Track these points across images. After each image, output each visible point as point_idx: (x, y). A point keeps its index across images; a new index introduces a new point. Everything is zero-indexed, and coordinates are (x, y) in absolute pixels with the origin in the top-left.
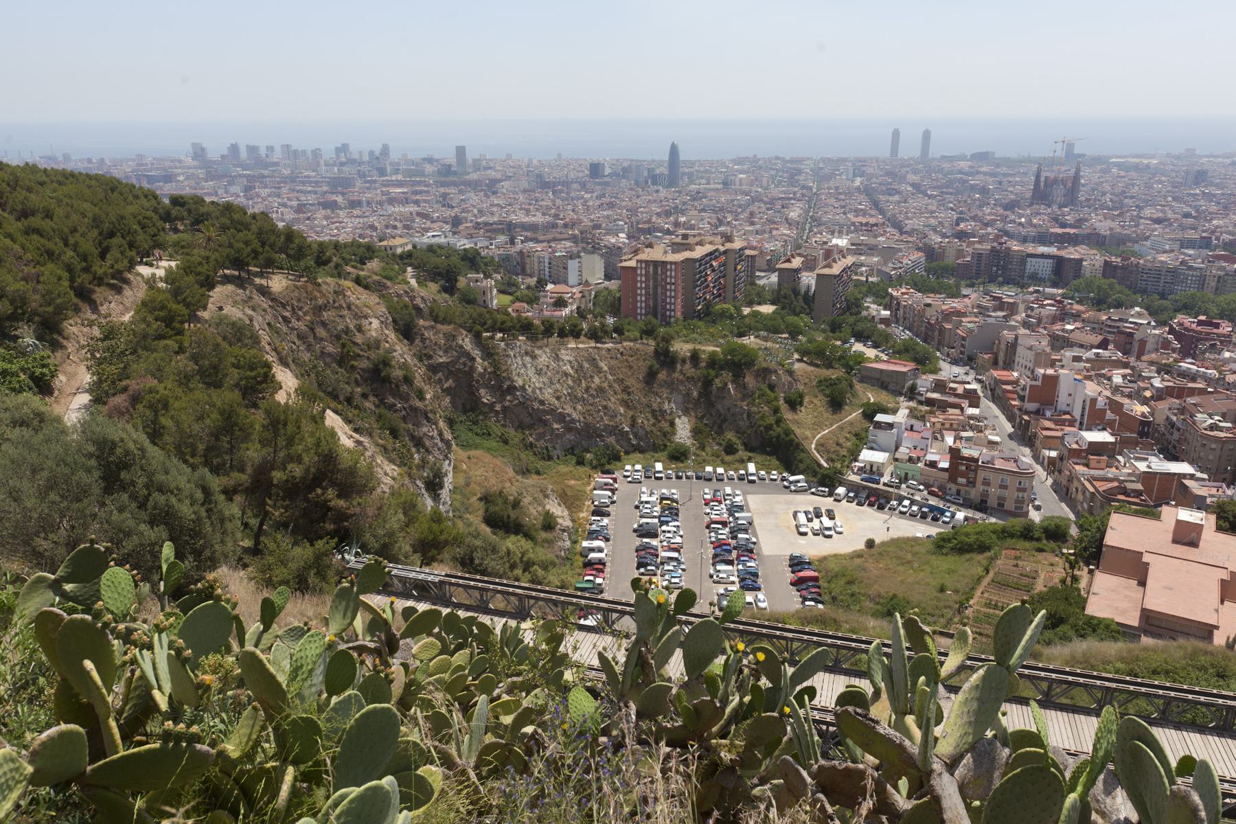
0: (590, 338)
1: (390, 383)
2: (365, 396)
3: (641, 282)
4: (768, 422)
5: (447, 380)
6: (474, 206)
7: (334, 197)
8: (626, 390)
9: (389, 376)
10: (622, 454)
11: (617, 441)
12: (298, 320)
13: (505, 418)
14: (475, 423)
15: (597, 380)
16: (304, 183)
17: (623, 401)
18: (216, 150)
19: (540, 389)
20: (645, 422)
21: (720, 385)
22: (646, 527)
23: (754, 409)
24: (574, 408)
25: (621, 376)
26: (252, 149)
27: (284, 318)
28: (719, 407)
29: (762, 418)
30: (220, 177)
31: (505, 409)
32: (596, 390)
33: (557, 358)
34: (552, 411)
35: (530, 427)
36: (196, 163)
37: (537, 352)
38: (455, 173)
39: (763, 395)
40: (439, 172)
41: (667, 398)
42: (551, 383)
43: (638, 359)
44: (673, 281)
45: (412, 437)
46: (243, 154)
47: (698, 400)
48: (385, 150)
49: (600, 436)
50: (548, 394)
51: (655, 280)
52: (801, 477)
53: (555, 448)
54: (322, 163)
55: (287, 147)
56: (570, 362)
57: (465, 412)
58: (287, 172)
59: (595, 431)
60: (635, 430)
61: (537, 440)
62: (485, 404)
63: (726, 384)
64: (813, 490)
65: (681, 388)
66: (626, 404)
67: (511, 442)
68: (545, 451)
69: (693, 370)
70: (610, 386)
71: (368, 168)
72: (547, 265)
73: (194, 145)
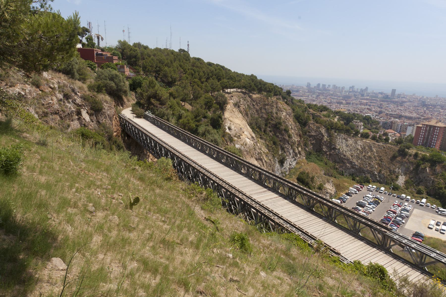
1: (279, 129)
3: (423, 132)
4: (441, 186)
5: (313, 140)
6: (390, 109)
7: (342, 101)
8: (381, 160)
9: (279, 127)
10: (371, 181)
11: (371, 177)
12: (257, 106)
13: (330, 157)
15: (369, 154)
16: (335, 96)
17: (378, 163)
18: (313, 85)
19: (346, 151)
20: (385, 173)
21: (423, 167)
22: (361, 203)
23: (436, 180)
24: (357, 161)
25: (381, 155)
26: (324, 85)
27: (253, 104)
28: (421, 176)
29: (438, 184)
30: (311, 92)
31: (330, 154)
32: (368, 157)
33: (356, 143)
34: (348, 160)
35: (338, 163)
36: (307, 88)
37: (348, 139)
38: (389, 98)
40: (383, 97)
41: (398, 167)
42: (351, 150)
43: (390, 151)
44: (437, 134)
45: (281, 147)
47: (412, 171)
48: (367, 88)
49: (364, 173)
50: (348, 154)
51: (429, 133)
53: (346, 172)
54: (344, 91)
55: (334, 86)
56: (361, 145)
57: (316, 152)
58: (331, 93)
59: (363, 171)
61: (339, 167)
62: (324, 151)
63: (426, 167)
65: (406, 165)
66: (379, 165)
67: (328, 164)
68: (341, 172)
69: (414, 160)
70: (374, 157)
71: (358, 94)
72: (400, 127)
73: (308, 83)
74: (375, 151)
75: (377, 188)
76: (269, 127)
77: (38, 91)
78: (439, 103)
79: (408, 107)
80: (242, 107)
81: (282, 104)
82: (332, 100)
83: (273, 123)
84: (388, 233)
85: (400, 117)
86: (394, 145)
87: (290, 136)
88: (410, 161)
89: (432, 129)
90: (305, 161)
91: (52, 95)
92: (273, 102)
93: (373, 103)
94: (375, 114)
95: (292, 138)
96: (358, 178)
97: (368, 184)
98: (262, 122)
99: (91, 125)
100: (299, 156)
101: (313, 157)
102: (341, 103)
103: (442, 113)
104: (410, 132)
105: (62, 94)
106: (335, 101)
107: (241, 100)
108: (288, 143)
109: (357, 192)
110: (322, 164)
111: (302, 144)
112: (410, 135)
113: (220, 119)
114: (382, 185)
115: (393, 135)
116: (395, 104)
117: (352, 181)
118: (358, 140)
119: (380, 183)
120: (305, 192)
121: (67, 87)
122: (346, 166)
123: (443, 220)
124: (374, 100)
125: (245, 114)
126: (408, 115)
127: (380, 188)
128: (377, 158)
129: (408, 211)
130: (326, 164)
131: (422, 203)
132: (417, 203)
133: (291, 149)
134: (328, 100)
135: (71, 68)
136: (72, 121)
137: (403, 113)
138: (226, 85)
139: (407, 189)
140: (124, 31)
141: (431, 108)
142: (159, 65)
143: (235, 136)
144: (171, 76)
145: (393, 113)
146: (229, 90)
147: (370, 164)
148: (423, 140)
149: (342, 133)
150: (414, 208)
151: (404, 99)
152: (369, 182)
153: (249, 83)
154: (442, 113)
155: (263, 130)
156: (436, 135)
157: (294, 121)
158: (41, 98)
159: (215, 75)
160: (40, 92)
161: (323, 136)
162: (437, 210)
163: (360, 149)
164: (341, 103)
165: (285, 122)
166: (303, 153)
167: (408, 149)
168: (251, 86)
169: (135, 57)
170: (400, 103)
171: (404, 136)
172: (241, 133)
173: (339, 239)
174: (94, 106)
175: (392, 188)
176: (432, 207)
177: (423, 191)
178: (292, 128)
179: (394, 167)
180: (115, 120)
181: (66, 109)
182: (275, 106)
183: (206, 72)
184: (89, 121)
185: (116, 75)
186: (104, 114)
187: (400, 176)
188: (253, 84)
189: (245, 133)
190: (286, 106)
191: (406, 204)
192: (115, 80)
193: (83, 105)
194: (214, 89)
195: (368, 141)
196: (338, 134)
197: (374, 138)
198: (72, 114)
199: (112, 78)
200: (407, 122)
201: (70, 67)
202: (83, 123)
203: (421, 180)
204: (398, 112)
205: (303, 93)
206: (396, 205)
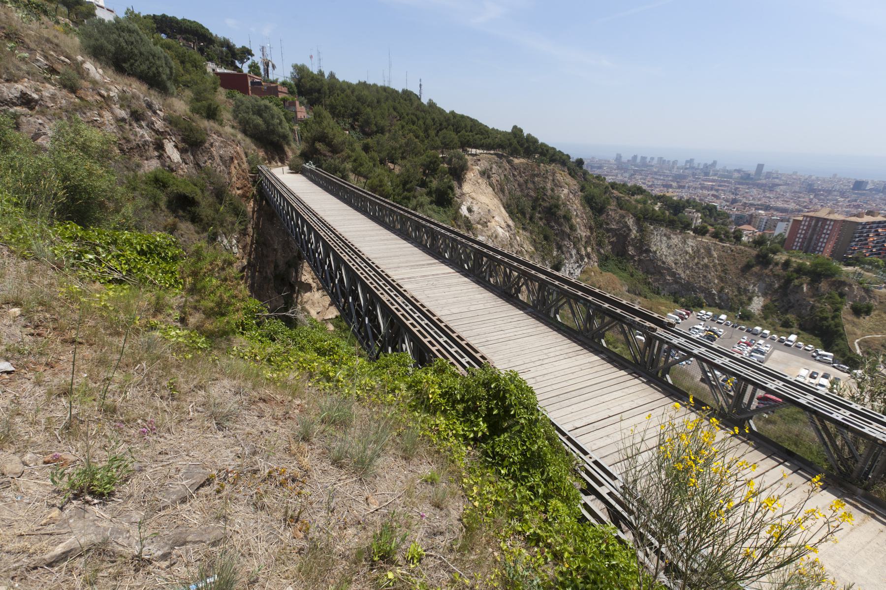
0: (713, 237)
1: (556, 216)
2: (541, 219)
4: (825, 315)
5: (613, 237)
6: (752, 196)
7: (671, 183)
8: (725, 271)
9: (555, 212)
11: (705, 298)
13: (638, 265)
14: (620, 262)
15: (706, 260)
16: (660, 175)
19: (666, 256)
20: (730, 293)
21: (797, 284)
24: (684, 272)
25: (725, 263)
26: (644, 158)
27: (513, 174)
28: (791, 298)
31: (640, 260)
33: (684, 242)
34: (669, 269)
35: (652, 274)
37: (672, 236)
38: (752, 179)
39: (830, 298)
40: (742, 178)
41: (753, 283)
45: (557, 244)
46: (639, 160)
48: (715, 163)
49: (695, 291)
50: (670, 260)
51: (814, 230)
52: (832, 354)
53: (663, 289)
55: (660, 159)
56: (692, 247)
57: (617, 255)
58: (655, 170)
59: (692, 288)
60: (721, 295)
61: (654, 282)
63: (802, 284)
64: (835, 365)
65: (767, 279)
66: (721, 279)
67: (635, 276)
70: (714, 266)
73: (617, 154)
74: (716, 256)
75: (714, 316)
76: (539, 213)
77: (72, 98)
78: (838, 187)
79: (782, 193)
80: (495, 178)
81: (562, 176)
82: (656, 182)
83: (545, 205)
84: (660, 331)
85: (767, 208)
86: (750, 247)
87: (572, 228)
88: (776, 273)
89: (820, 223)
90: (598, 269)
91: (101, 108)
92: (547, 171)
93: (723, 186)
94: (724, 203)
95: (575, 230)
96: (683, 300)
97: (699, 309)
98: (527, 204)
99: (182, 169)
100: (586, 260)
101: (611, 264)
102: (671, 186)
103: (841, 204)
104: (782, 229)
105: (128, 110)
106: (659, 182)
107: (494, 166)
108: (569, 239)
109: (680, 321)
110: (625, 275)
111: (593, 242)
112: (780, 234)
113: (450, 191)
114: (723, 311)
115: (749, 233)
116: (760, 188)
117: (673, 304)
118: (688, 238)
119: (720, 307)
120: (499, 257)
121: (138, 99)
122: (665, 279)
123: (823, 370)
124: (725, 182)
125: (499, 190)
126: (782, 205)
127: (719, 316)
128: (719, 268)
129: (762, 353)
130: (632, 276)
131: (789, 341)
132: (781, 341)
133: (574, 248)
134: (649, 181)
135: (156, 72)
136: (147, 159)
137: (773, 203)
138: (468, 141)
139: (765, 318)
140: (311, 57)
141: (822, 195)
142: (358, 104)
143: (478, 223)
144: (376, 122)
145: (756, 202)
146: (474, 151)
147: (705, 276)
148: (803, 242)
149: (662, 225)
150: (774, 349)
151: (777, 181)
152: (701, 306)
153: (509, 140)
154: (841, 204)
155: (528, 216)
156: (826, 234)
157: (582, 205)
158: (76, 110)
159: (453, 126)
160: (77, 100)
161: (630, 230)
162: (814, 354)
163: (691, 252)
164: (671, 186)
165: (565, 205)
166: (594, 257)
167: (775, 253)
168: (511, 144)
169: (319, 91)
170: (769, 187)
171: (770, 236)
172: (489, 217)
173: (544, 347)
174: (188, 136)
175: (740, 315)
176: (807, 348)
177: (793, 323)
178: (577, 215)
179: (746, 282)
180: (238, 167)
181: (132, 137)
182: (551, 178)
183: (436, 119)
184: (178, 162)
185: (266, 107)
186: (207, 151)
187: (756, 298)
188: (515, 141)
189: (497, 218)
190: (569, 179)
191: (761, 341)
192: (264, 114)
193: (166, 131)
194: (448, 145)
195: (706, 239)
196: (654, 228)
197: (716, 236)
198: (147, 147)
199: (259, 112)
200: (777, 216)
201: (154, 69)
202: (167, 164)
203: (791, 305)
204: (764, 200)
205: (609, 170)
206: (744, 343)
